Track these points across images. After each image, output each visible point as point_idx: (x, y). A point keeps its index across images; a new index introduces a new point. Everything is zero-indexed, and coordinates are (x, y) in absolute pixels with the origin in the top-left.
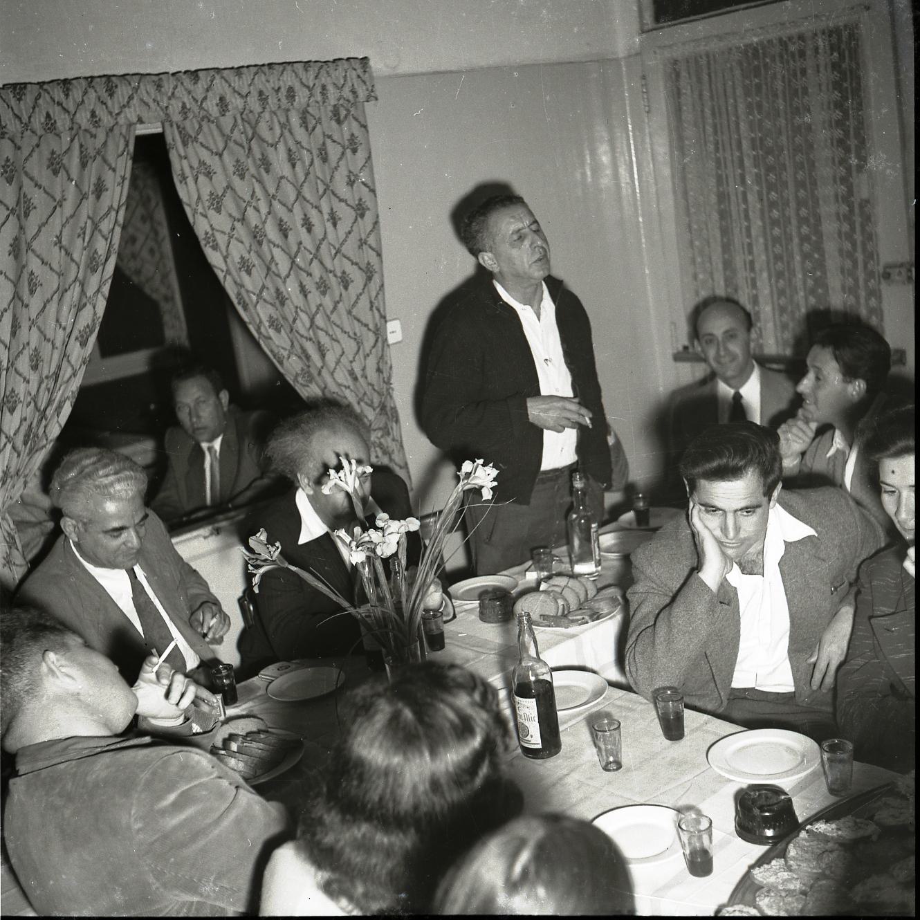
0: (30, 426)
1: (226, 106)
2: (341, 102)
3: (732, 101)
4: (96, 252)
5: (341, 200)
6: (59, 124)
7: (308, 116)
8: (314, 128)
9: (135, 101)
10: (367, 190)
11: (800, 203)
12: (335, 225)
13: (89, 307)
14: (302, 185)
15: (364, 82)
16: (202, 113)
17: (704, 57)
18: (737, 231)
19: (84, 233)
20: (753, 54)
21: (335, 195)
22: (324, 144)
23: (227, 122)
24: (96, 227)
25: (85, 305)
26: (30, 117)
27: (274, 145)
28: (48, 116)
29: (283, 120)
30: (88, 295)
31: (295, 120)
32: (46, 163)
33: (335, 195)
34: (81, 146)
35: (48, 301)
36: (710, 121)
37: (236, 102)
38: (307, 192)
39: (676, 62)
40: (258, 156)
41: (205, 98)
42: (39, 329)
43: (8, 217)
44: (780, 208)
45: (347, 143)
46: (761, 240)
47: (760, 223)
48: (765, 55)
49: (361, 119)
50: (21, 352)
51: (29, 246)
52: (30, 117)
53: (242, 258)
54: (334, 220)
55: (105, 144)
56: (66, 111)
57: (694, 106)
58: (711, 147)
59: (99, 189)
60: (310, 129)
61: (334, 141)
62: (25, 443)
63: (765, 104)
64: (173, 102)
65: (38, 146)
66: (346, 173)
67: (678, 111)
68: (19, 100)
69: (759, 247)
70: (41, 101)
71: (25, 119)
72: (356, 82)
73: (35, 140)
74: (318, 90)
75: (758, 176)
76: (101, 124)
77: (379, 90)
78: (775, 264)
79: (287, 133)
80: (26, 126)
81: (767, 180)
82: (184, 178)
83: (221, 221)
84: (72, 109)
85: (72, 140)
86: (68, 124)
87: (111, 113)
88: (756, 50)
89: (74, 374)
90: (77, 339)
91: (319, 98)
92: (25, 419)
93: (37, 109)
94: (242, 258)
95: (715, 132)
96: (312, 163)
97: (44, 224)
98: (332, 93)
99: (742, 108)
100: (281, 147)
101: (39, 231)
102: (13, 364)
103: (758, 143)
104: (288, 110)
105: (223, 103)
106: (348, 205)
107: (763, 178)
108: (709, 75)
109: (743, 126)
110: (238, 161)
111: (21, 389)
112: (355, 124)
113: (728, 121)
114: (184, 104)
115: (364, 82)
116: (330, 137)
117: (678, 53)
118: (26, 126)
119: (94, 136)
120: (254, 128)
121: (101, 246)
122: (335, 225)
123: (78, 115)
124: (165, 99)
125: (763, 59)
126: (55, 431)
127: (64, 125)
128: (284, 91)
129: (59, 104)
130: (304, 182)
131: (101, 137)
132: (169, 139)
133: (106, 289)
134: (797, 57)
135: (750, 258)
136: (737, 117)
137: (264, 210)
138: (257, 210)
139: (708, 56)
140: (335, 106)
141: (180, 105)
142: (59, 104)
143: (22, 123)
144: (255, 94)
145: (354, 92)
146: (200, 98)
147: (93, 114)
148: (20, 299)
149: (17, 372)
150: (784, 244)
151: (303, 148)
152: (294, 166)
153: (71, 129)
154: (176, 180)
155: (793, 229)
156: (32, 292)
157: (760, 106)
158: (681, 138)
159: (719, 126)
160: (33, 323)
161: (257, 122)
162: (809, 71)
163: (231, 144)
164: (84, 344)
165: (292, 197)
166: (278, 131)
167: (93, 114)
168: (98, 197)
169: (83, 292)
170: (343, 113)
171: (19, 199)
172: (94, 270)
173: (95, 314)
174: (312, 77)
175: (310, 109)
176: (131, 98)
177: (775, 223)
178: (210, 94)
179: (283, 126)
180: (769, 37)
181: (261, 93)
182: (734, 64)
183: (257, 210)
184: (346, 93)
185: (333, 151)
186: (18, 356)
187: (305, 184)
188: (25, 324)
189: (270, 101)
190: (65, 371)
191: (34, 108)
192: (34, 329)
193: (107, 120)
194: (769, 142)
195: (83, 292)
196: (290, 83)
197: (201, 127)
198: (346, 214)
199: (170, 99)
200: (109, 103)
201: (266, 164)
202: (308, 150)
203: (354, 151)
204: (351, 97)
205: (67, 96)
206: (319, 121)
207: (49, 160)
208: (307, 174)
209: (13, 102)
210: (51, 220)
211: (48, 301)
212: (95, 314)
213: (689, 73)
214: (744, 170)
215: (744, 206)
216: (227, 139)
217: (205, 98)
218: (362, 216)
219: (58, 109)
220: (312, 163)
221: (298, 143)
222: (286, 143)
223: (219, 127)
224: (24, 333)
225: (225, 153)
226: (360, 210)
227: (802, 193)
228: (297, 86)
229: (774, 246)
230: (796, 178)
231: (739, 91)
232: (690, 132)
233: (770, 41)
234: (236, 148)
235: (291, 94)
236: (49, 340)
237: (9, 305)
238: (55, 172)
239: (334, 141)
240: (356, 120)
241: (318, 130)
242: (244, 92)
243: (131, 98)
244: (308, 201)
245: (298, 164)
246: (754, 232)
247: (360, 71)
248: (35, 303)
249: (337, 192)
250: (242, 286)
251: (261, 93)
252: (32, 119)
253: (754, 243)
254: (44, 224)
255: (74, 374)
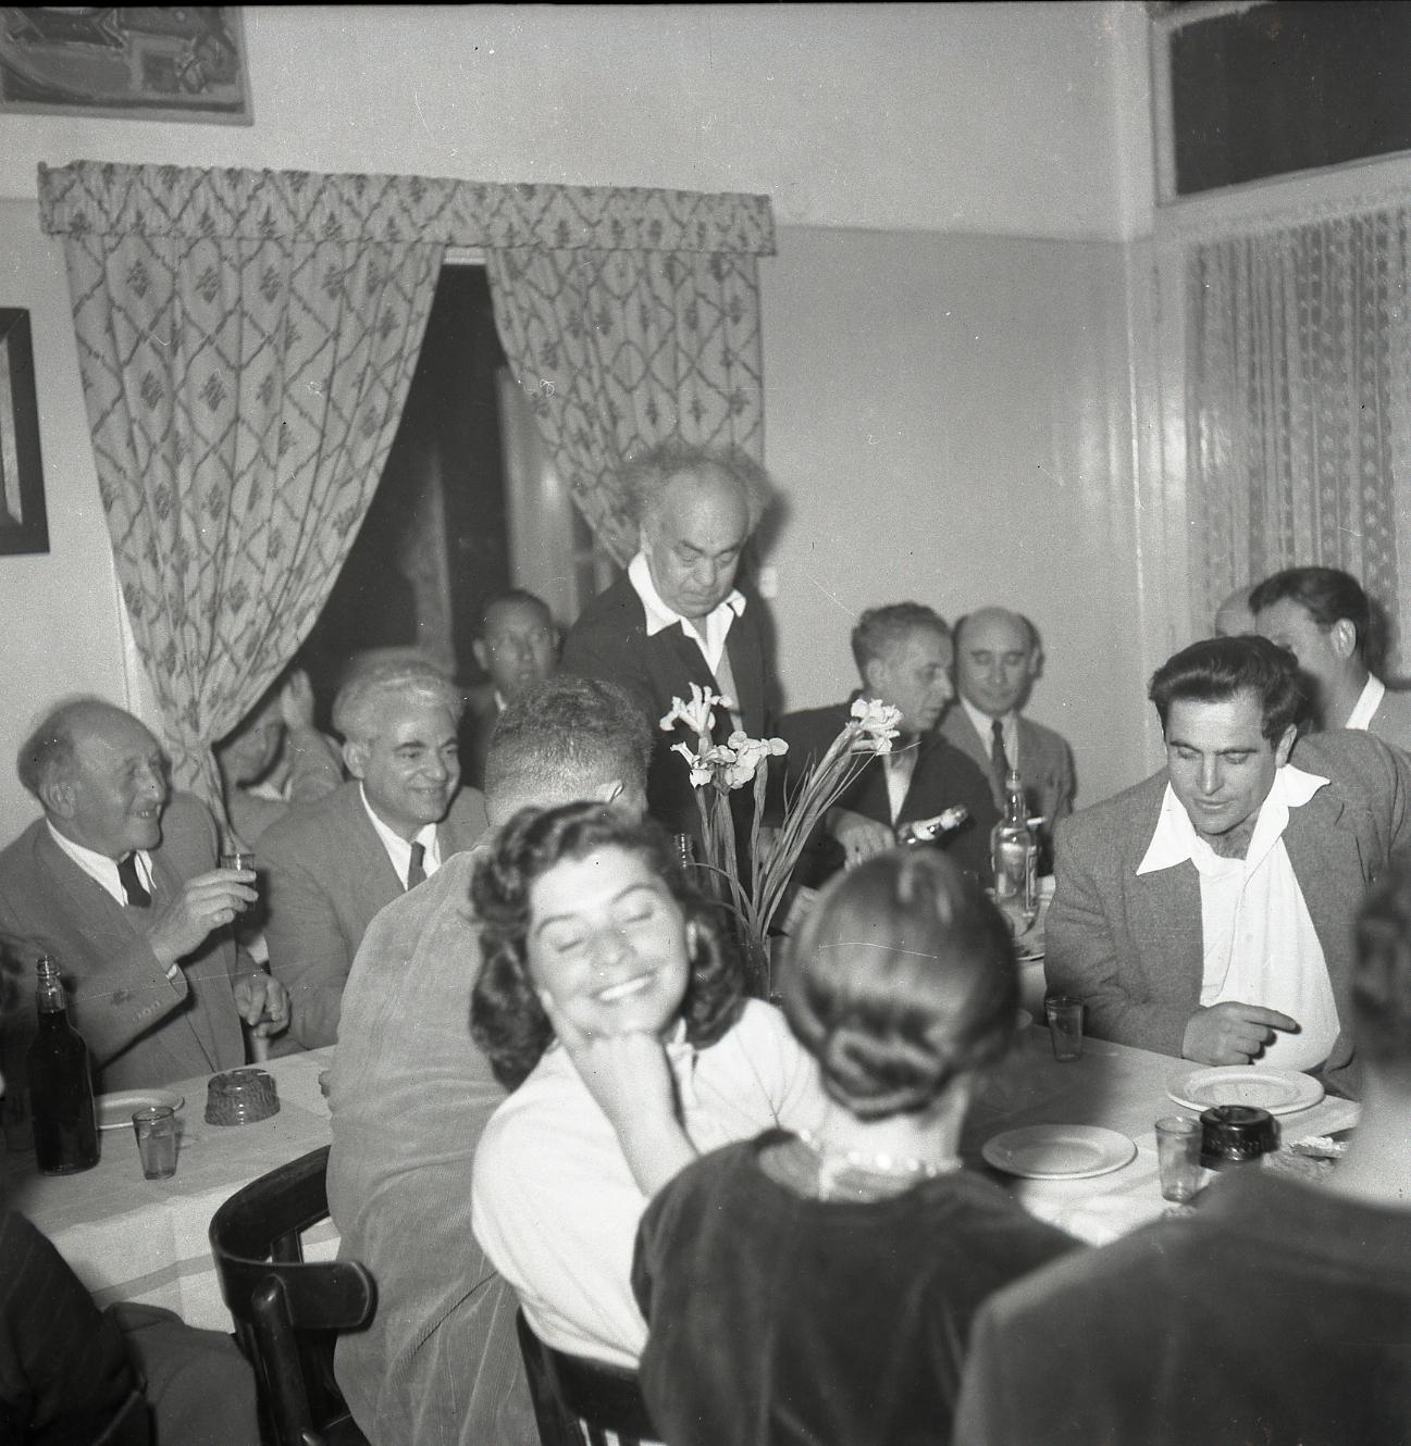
0: (258, 634)
1: (567, 234)
2: (725, 249)
3: (1280, 355)
4: (373, 410)
5: (710, 385)
6: (346, 230)
7: (677, 264)
8: (683, 281)
9: (447, 214)
10: (748, 375)
11: (1365, 455)
12: (698, 418)
13: (356, 483)
14: (652, 358)
15: (758, 226)
16: (534, 241)
17: (1244, 243)
18: (1272, 495)
19: (362, 381)
20: (1313, 240)
21: (702, 376)
22: (695, 303)
23: (564, 259)
24: (377, 376)
25: (350, 480)
26: (308, 215)
27: (624, 300)
28: (332, 217)
29: (640, 265)
30: (357, 466)
31: (657, 267)
32: (321, 280)
33: (702, 376)
34: (371, 264)
35: (302, 466)
36: (1246, 335)
37: (581, 233)
38: (658, 367)
39: (1201, 250)
40: (596, 309)
41: (539, 221)
42: (286, 503)
43: (262, 347)
44: (1336, 462)
45: (727, 308)
46: (1306, 508)
47: (1305, 482)
48: (1329, 241)
49: (750, 277)
50: (259, 530)
51: (285, 389)
52: (308, 215)
53: (580, 430)
54: (697, 411)
55: (401, 266)
56: (356, 214)
57: (1223, 310)
58: (1244, 372)
59: (387, 327)
60: (677, 282)
61: (709, 302)
62: (248, 656)
63: (1325, 310)
64: (496, 220)
65: (313, 256)
66: (721, 347)
67: (1198, 318)
68: (297, 190)
69: (1302, 485)
70: (324, 197)
71: (302, 216)
72: (748, 225)
73: (310, 248)
74: (693, 229)
75: (1309, 416)
76: (399, 237)
77: (781, 243)
78: (1321, 490)
79: (643, 284)
80: (302, 227)
81: (1320, 420)
82: (509, 321)
83: (551, 382)
84: (365, 213)
85: (359, 256)
86: (358, 232)
87: (413, 224)
88: (1316, 235)
89: (327, 572)
90: (335, 524)
91: (695, 240)
92: (253, 623)
93: (319, 207)
94: (580, 430)
95: (1252, 351)
96: (673, 328)
97: (308, 362)
98: (713, 234)
99: (1292, 316)
100: (633, 302)
101: (301, 370)
102: (245, 546)
103: (1311, 364)
104: (648, 251)
105: (563, 230)
106: (719, 393)
107: (1315, 417)
108: (1249, 269)
109: (1293, 342)
110: (572, 313)
111: (253, 582)
112: (740, 283)
113: (1271, 334)
114: (511, 225)
115: (758, 226)
116: (703, 296)
117: (1206, 236)
118: (302, 227)
119: (389, 254)
120: (598, 271)
121: (380, 402)
122: (698, 418)
123: (370, 222)
124: (487, 215)
125: (1328, 247)
126: (289, 647)
127: (352, 232)
128: (646, 225)
129: (349, 203)
130: (656, 352)
131: (398, 257)
132: (492, 272)
133: (381, 462)
134: (1375, 245)
135: (1289, 533)
136: (1284, 327)
137: (597, 383)
138: (590, 380)
139: (1248, 241)
140: (714, 254)
141: (506, 225)
142: (349, 203)
143: (296, 222)
144: (607, 222)
145: (743, 238)
146: (534, 218)
147: (391, 223)
148: (266, 458)
149: (249, 556)
150: (1338, 514)
151: (663, 306)
152: (645, 327)
153: (360, 239)
154: (500, 325)
155: (1352, 494)
156: (281, 452)
157: (1317, 313)
158: (1200, 356)
159: (1257, 343)
160: (276, 494)
161: (603, 264)
162: (1391, 265)
163: (567, 289)
164: (343, 533)
165: (638, 371)
166: (631, 277)
167: (391, 223)
168: (385, 336)
169: (350, 462)
170: (725, 267)
171: (280, 322)
172: (368, 434)
173: (362, 494)
174: (688, 210)
175: (679, 255)
176: (442, 208)
177: (1326, 482)
178: (547, 216)
179: (639, 272)
180: (1336, 216)
181: (616, 223)
182: (1286, 253)
183: (590, 380)
184: (732, 238)
185: (707, 316)
186: (253, 535)
187: (658, 357)
188: (268, 495)
189: (627, 235)
190: (314, 567)
191: (315, 203)
192: (279, 503)
193: (408, 234)
194: (1327, 339)
195: (350, 462)
196: (656, 216)
197: (530, 259)
198: (715, 405)
199: (493, 215)
200: (414, 211)
201: (605, 322)
202: (669, 310)
203: (736, 320)
204: (738, 244)
205: (360, 193)
206: (691, 272)
207: (327, 276)
208: (663, 343)
209: (289, 192)
210: (318, 357)
211: (302, 466)
212: (362, 494)
213: (1220, 265)
214: (1288, 406)
215: (1285, 457)
216: (562, 280)
217: (539, 221)
218: (739, 411)
219: (346, 209)
220: (673, 328)
221: (656, 298)
222: (640, 296)
223: (554, 263)
224: (264, 506)
225: (559, 299)
226: (736, 403)
227: (1369, 441)
228: (666, 220)
229: (1323, 514)
230: (1362, 446)
231: (1290, 292)
232: (1212, 349)
233: (1338, 223)
234: (572, 293)
235: (656, 230)
236: (296, 519)
237: (249, 466)
238: (332, 294)
239: (709, 302)
240: (742, 276)
241: (688, 283)
242: (595, 219)
243: (442, 208)
244: (657, 380)
245: (652, 328)
246: (1296, 496)
247: (754, 211)
248: (286, 466)
249: (705, 372)
250: (580, 464)
251: (616, 223)
252: (311, 218)
253: (1296, 511)
254: (308, 362)
255: (327, 572)
